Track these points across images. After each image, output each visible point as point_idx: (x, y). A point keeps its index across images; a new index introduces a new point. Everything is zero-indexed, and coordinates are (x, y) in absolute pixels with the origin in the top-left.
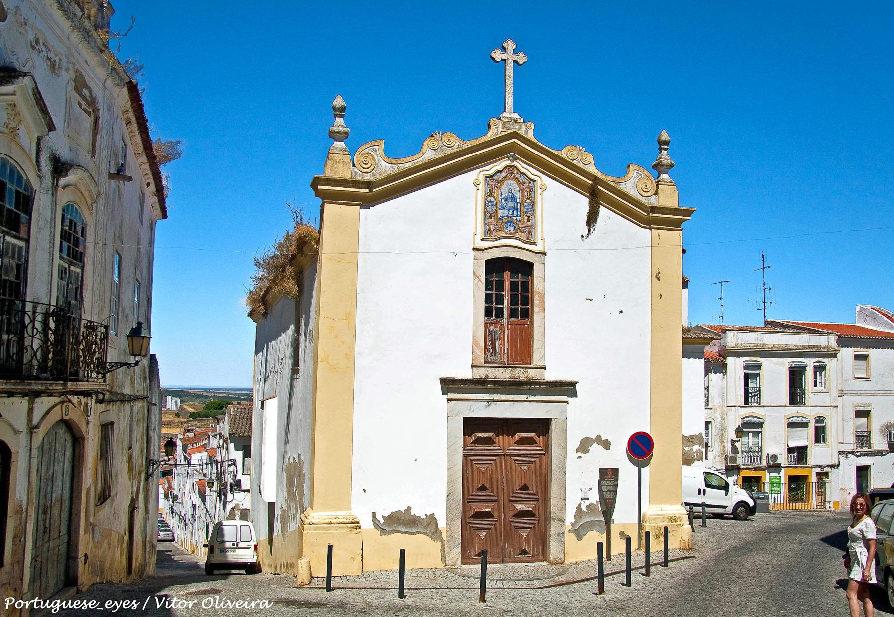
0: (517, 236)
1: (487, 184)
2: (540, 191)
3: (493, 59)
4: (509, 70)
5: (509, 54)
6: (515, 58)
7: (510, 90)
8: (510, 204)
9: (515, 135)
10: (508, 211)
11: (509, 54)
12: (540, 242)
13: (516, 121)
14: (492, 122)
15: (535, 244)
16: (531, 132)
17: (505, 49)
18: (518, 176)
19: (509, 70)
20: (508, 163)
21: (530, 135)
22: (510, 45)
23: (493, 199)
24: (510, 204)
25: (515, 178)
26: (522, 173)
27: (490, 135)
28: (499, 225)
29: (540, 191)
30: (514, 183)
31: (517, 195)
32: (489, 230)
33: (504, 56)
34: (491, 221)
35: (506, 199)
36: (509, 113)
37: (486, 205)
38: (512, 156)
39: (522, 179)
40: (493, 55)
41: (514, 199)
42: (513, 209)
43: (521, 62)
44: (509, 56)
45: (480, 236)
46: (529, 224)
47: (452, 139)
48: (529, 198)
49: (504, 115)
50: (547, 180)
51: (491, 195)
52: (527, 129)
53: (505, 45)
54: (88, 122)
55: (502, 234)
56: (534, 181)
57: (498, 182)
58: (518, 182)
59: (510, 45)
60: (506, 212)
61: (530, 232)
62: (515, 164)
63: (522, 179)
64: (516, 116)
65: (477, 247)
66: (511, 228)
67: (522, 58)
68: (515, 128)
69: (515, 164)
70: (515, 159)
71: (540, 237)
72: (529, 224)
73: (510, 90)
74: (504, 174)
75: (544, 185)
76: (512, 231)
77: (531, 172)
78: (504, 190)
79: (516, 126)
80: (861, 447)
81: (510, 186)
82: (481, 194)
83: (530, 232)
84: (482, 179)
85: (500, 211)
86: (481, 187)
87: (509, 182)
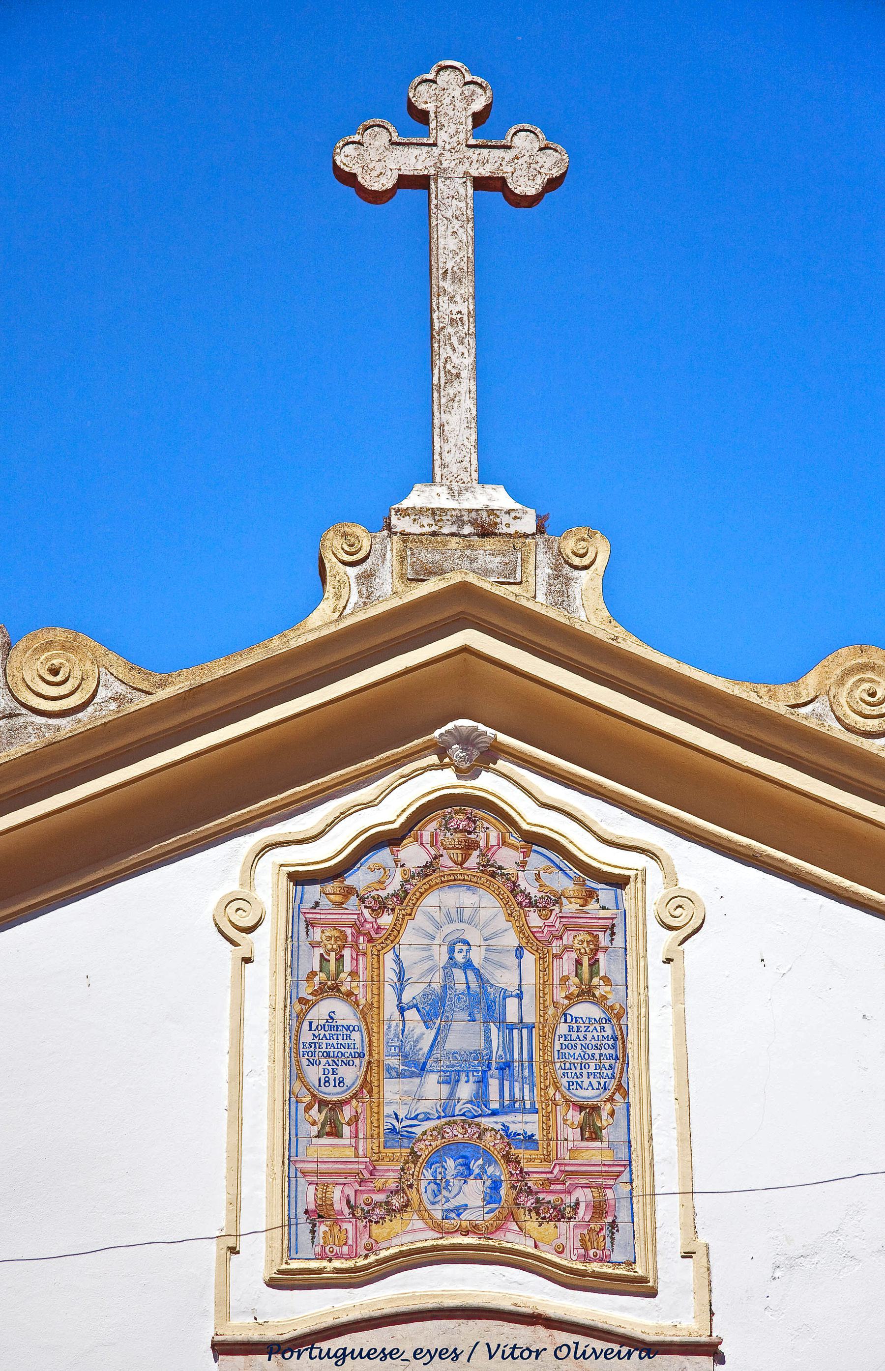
0: (512, 1239)
1: (301, 920)
2: (659, 941)
3: (349, 179)
4: (453, 243)
5: (449, 142)
6: (489, 163)
7: (458, 355)
8: (463, 1036)
9: (465, 606)
10: (451, 1080)
11: (449, 142)
12: (673, 1274)
13: (486, 531)
14: (334, 546)
15: (642, 1287)
16: (587, 586)
17: (422, 117)
18: (507, 858)
19: (453, 243)
20: (444, 780)
21: (587, 609)
22: (451, 95)
23: (343, 1012)
24: (463, 1036)
25: (491, 871)
26: (534, 840)
27: (321, 621)
28: (389, 1178)
29: (659, 941)
30: (485, 905)
31: (505, 979)
32: (320, 1214)
33: (414, 161)
34: (329, 1150)
35: (434, 1009)
36: (455, 486)
37: (296, 1056)
38: (467, 740)
39: (534, 874)
40: (346, 158)
41: (486, 1005)
42: (482, 1067)
43: (525, 185)
44: (451, 156)
45: (258, 1258)
46: (595, 1153)
47: (74, 666)
48: (586, 994)
49: (417, 498)
50: (699, 869)
51: (331, 989)
52: (564, 567)
53: (423, 97)
54: (376, 129)
55: (414, 1233)
56: (619, 882)
57: (380, 907)
58: (515, 899)
59: (451, 95)
60: (432, 1087)
61: (599, 1209)
62: (487, 783)
63: (534, 874)
64: (498, 498)
65: (241, 1328)
66: (472, 1193)
67: (528, 160)
68: (480, 568)
69: (487, 783)
70: (489, 756)
71: (670, 1238)
72: (595, 1153)
73: (458, 355)
74: (414, 855)
75: (680, 899)
76: (478, 1214)
77: (596, 825)
78: (418, 950)
79: (488, 554)
80: (586, 1259)
81: (460, 924)
82: (264, 984)
83: (599, 1209)
84: (269, 890)
85: (391, 1089)
86: (265, 944)
87: (451, 898)
